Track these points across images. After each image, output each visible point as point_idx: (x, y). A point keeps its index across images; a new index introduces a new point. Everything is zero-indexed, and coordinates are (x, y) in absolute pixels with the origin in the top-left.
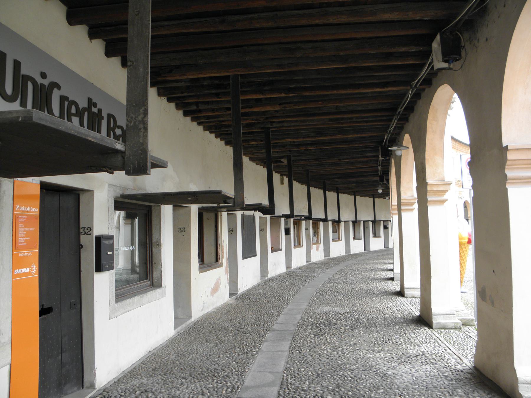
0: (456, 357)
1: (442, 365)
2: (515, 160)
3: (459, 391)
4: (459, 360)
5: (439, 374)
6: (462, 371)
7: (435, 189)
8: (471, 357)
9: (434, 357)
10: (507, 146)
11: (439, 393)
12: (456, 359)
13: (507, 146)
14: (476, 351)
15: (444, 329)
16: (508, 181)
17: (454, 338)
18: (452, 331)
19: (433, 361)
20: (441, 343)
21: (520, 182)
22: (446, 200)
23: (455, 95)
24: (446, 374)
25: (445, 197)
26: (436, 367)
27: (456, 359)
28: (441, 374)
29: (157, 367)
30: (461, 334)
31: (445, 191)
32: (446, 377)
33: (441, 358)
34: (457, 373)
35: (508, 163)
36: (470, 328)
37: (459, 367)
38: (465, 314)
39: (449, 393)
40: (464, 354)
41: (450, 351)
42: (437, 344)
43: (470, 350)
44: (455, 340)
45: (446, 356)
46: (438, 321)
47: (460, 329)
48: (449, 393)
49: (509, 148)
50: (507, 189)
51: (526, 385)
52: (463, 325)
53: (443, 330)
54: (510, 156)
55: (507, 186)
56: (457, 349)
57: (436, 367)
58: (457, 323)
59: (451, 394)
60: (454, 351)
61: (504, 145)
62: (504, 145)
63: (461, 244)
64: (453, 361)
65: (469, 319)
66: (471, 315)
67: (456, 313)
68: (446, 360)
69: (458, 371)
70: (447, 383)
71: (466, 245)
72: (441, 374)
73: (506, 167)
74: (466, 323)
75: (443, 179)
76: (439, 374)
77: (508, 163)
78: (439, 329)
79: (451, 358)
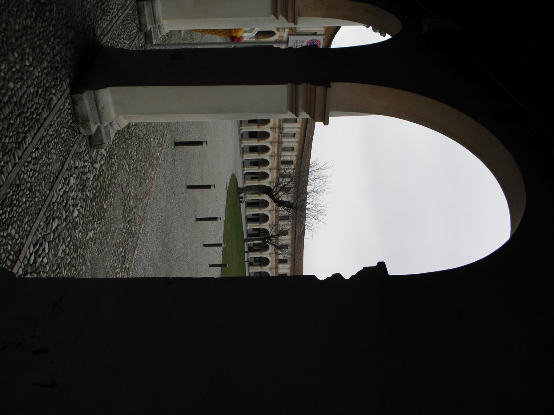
0: (109, 27)
1: (98, 14)
2: (315, 93)
3: (73, 34)
4: (106, 32)
5: (86, 11)
6: (95, 35)
7: (290, 6)
8: (111, 43)
9: (105, 4)
10: (330, 87)
11: (64, 12)
12: (106, 27)
13: (330, 87)
14: (119, 49)
15: (139, 14)
16: (294, 85)
17: (130, 25)
18: (137, 22)
19: (100, 3)
20: (121, 11)
21: (296, 101)
22: (277, 18)
23: (388, 37)
24: (88, 19)
25: (281, 17)
26: (94, 6)
27: (106, 27)
28: (87, 13)
29: (29, 278)
30: (135, 31)
31: (286, 17)
32: (84, 19)
33: (106, 12)
34: (92, 30)
35: (313, 87)
36: (143, 40)
37: (99, 32)
38: (157, 35)
39: (68, 23)
40: (114, 36)
41: (114, 21)
42: (119, 7)
43: (119, 42)
44: (127, 25)
45: (109, 17)
46: (145, 7)
47: (141, 30)
48: (68, 23)
49: (328, 89)
50: (287, 84)
51: (93, 97)
52: (145, 33)
53: (136, 12)
54: (320, 90)
55: (289, 84)
56: (118, 28)
57: (94, 6)
58: (146, 27)
59: (67, 25)
60: (115, 26)
61: (332, 84)
62: (332, 84)
63: (230, 30)
64: (105, 25)
65: (152, 39)
66: (157, 42)
67: (157, 25)
68: (104, 18)
69: (94, 31)
70: (78, 20)
71: (229, 35)
72: (87, 13)
73: (309, 84)
74: (148, 36)
75: (300, 15)
76: (86, 11)
77: (313, 87)
78: (138, 8)
79: (107, 23)
